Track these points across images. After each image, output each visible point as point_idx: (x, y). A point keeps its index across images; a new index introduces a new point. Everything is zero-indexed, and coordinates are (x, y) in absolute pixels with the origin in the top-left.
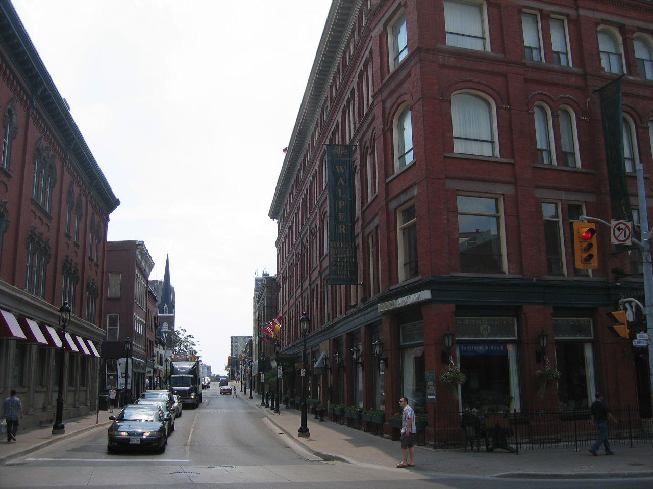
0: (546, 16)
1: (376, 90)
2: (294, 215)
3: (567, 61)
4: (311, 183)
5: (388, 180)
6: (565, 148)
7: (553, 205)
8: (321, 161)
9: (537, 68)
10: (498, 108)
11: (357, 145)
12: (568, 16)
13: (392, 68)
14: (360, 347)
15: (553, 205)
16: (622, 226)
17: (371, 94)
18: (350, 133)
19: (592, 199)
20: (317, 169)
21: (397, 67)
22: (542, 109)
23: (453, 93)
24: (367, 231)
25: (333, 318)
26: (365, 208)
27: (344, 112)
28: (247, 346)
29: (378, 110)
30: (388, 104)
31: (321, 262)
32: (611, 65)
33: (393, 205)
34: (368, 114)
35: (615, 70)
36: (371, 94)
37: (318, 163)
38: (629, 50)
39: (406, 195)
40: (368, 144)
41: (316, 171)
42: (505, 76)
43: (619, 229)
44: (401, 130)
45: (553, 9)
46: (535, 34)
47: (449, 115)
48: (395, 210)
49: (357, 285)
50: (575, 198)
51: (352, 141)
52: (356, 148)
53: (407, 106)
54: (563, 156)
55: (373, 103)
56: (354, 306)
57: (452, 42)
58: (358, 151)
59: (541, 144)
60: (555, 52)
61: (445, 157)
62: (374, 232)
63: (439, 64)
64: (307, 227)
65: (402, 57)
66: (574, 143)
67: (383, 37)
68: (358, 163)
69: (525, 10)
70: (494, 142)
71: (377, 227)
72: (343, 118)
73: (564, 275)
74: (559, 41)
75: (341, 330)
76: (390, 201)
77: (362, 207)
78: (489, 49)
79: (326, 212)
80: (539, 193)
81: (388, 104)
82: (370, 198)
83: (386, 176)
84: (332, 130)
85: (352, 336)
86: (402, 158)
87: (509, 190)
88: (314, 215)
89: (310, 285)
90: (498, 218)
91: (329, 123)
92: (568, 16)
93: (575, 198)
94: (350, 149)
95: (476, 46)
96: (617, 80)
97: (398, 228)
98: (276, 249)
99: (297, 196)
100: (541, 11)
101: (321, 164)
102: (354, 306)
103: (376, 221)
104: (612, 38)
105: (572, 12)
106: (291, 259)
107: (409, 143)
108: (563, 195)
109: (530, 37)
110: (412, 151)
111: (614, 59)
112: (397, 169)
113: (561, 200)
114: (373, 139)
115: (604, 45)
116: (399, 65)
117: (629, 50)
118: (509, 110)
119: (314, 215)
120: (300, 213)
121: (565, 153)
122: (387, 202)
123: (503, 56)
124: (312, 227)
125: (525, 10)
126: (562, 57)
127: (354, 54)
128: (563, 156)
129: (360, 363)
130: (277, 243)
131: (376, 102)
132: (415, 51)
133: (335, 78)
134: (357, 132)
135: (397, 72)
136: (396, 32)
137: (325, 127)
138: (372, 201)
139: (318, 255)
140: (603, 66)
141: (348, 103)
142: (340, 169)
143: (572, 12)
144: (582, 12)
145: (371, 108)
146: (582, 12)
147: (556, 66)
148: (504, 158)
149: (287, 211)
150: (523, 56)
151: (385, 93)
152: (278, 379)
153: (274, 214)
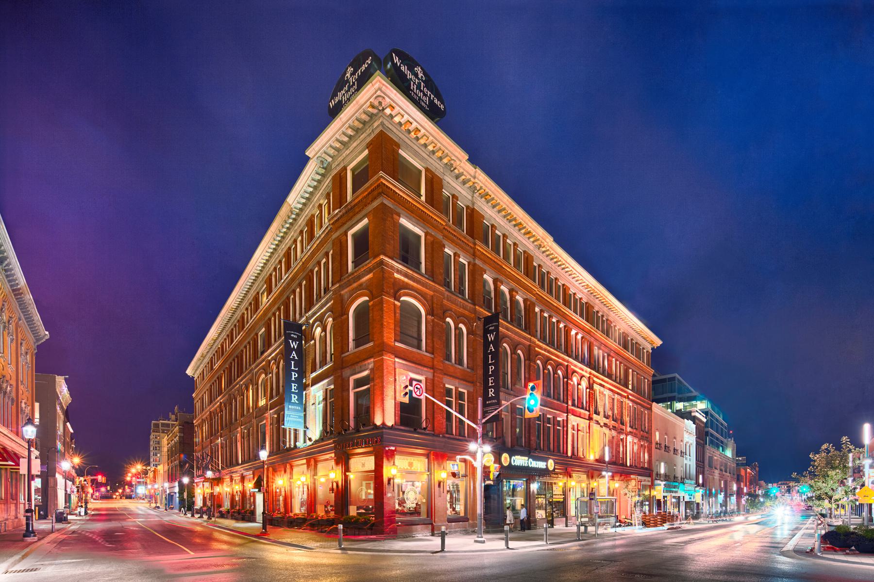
16: (419, 387)
43: (417, 388)
73: (465, 437)
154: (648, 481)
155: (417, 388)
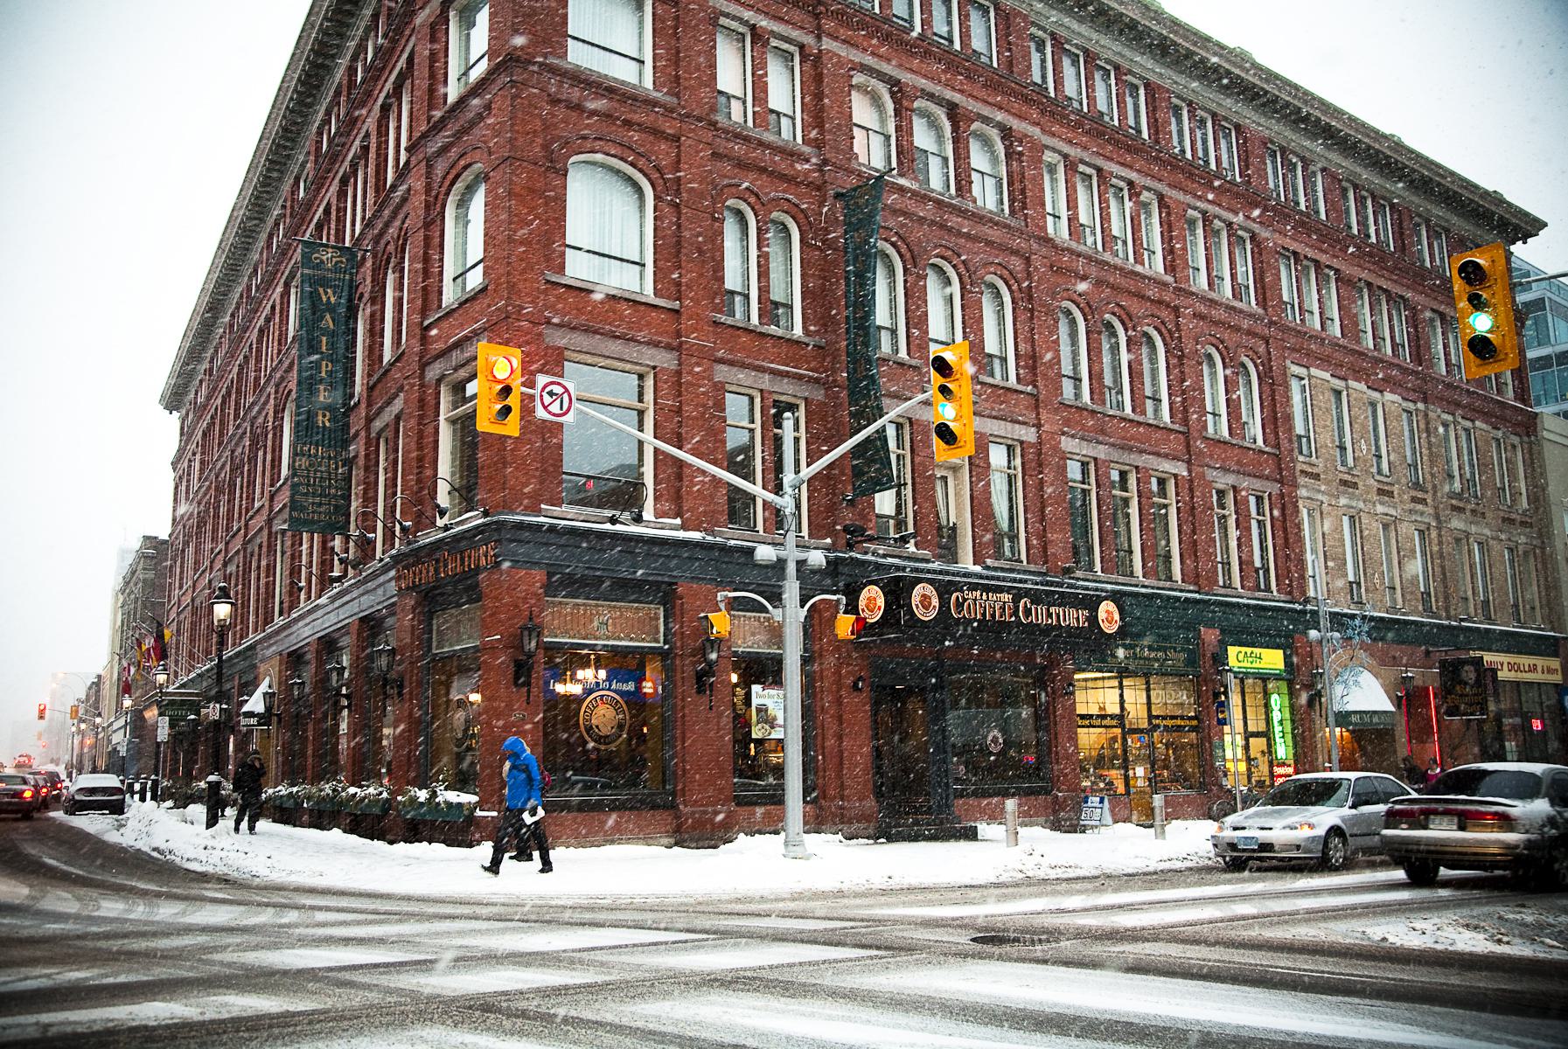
0: (758, 36)
1: (416, 135)
2: (219, 401)
3: (791, 132)
4: (261, 331)
5: (426, 323)
6: (777, 294)
7: (746, 398)
8: (287, 285)
9: (739, 136)
10: (657, 197)
11: (367, 251)
12: (802, 47)
13: (453, 92)
14: (345, 662)
15: (746, 398)
17: (404, 144)
18: (354, 227)
19: (819, 395)
20: (278, 301)
21: (462, 90)
22: (740, 215)
23: (573, 159)
24: (378, 424)
25: (291, 609)
26: (376, 377)
27: (344, 182)
28: (90, 688)
29: (416, 182)
30: (440, 168)
31: (272, 498)
32: (871, 153)
33: (433, 373)
34: (394, 187)
35: (878, 162)
36: (404, 144)
37: (279, 289)
38: (904, 131)
39: (462, 351)
40: (391, 248)
41: (273, 307)
42: (1176, 309)
43: (551, 394)
44: (461, 219)
45: (775, 29)
46: (739, 62)
47: (561, 200)
48: (439, 381)
49: (348, 538)
50: (787, 390)
51: (357, 242)
52: (364, 259)
53: (477, 176)
54: (770, 309)
55: (407, 163)
56: (339, 579)
57: (578, 56)
58: (369, 263)
59: (732, 281)
60: (772, 111)
61: (548, 282)
62: (392, 427)
63: (549, 95)
64: (247, 425)
65: (476, 73)
66: (789, 283)
67: (437, 30)
68: (367, 288)
69: (723, 21)
70: (644, 265)
71: (398, 418)
72: (342, 194)
74: (782, 91)
75: (307, 632)
76: (429, 363)
77: (370, 375)
78: (648, 83)
79: (291, 391)
80: (722, 373)
81: (440, 168)
82: (387, 356)
83: (424, 312)
84: (315, 220)
85: (328, 644)
86: (460, 280)
87: (666, 360)
88: (265, 395)
89: (245, 544)
90: (641, 413)
91: (309, 205)
92: (802, 47)
93: (787, 390)
94: (351, 256)
95: (622, 72)
96: (879, 183)
97: (442, 418)
98: (173, 475)
99: (231, 355)
100: (753, 28)
101: (286, 294)
102: (339, 579)
103: (398, 405)
104: (876, 100)
105: (808, 40)
106: (205, 494)
107: (476, 250)
108: (765, 381)
109: (730, 72)
110: (481, 265)
111: (876, 141)
112: (450, 296)
113: (761, 391)
114: (403, 238)
115: (862, 111)
116: (469, 87)
117: (904, 131)
118: (677, 206)
119: (265, 395)
120: (234, 396)
121: (776, 305)
122: (423, 366)
123: (675, 100)
124: (257, 424)
125: (723, 21)
126: (785, 122)
127: (373, 61)
128: (770, 309)
129: (344, 696)
130: (174, 465)
131: (413, 159)
132: (505, 62)
133: (328, 113)
134: (368, 225)
135: (462, 101)
136: (468, 23)
137: (301, 212)
138: (392, 364)
139: (267, 481)
140: (856, 150)
141: (354, 167)
142: (329, 296)
143: (808, 40)
144: (827, 44)
145: (402, 174)
146: (827, 44)
147: (769, 137)
148: (662, 297)
149: (204, 391)
150: (714, 109)
151: (433, 147)
152: (158, 745)
153: (173, 401)
154: (1550, 671)
155: (551, 394)
